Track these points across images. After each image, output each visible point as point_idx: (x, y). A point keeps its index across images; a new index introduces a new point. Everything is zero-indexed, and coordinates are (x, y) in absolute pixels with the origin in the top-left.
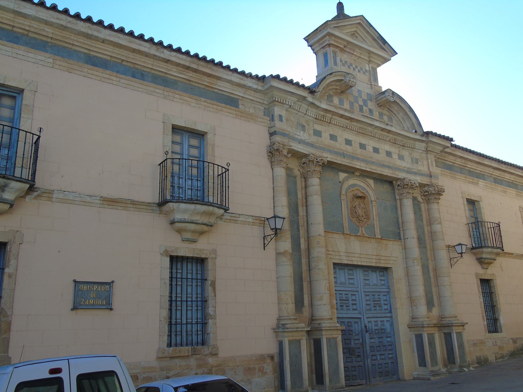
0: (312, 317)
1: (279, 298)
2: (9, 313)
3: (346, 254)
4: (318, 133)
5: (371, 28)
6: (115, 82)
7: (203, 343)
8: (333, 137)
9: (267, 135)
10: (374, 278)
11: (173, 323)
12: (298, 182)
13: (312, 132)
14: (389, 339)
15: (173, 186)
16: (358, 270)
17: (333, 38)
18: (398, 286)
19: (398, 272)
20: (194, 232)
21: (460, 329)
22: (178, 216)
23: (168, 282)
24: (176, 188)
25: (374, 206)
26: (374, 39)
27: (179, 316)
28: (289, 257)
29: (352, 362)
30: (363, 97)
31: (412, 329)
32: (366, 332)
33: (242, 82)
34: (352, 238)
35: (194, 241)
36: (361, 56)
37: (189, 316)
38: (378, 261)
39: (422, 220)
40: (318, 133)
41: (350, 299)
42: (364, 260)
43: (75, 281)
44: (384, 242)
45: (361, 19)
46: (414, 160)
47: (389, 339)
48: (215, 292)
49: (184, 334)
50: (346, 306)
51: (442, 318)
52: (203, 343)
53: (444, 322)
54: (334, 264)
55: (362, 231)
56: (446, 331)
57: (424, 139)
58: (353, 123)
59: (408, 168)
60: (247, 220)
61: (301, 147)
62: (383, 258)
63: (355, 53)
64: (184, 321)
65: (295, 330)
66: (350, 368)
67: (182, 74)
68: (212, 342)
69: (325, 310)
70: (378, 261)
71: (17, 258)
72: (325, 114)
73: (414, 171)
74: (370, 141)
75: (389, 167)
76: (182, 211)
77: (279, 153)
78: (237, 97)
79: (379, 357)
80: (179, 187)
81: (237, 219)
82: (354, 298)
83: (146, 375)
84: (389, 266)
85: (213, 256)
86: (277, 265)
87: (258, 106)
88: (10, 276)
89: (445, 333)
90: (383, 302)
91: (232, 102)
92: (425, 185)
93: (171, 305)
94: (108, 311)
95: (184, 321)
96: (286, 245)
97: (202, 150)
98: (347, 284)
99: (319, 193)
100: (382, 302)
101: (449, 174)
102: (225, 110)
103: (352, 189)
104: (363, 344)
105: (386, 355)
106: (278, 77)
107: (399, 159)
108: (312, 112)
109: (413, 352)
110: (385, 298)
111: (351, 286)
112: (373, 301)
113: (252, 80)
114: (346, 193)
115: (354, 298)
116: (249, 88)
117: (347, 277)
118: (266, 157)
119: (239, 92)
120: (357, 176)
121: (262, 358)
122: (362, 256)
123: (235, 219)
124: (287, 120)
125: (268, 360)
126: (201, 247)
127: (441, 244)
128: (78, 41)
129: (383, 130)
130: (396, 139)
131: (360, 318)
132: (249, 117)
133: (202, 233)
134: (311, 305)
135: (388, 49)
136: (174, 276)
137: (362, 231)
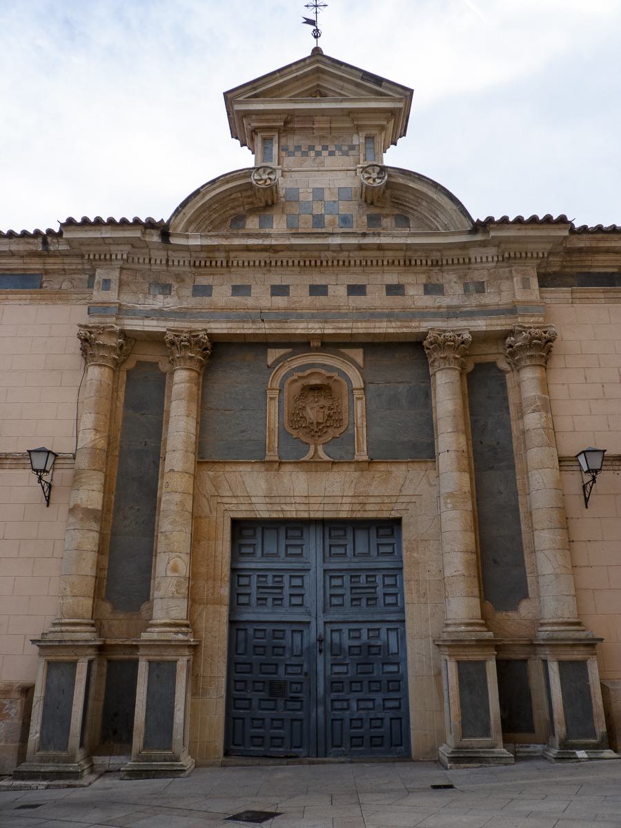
3: (268, 500)
8: (238, 290)
26: (358, 85)
42: (316, 507)
44: (382, 467)
57: (479, 237)
59: (448, 307)
61: (154, 323)
62: (372, 500)
70: (358, 507)
72: (210, 255)
75: (390, 316)
79: (354, 705)
82: (297, 582)
101: (602, 295)
102: (11, 296)
106: (70, 222)
110: (388, 581)
111: (294, 559)
114: (282, 385)
115: (297, 582)
119: (35, 265)
122: (312, 500)
135: (391, 90)
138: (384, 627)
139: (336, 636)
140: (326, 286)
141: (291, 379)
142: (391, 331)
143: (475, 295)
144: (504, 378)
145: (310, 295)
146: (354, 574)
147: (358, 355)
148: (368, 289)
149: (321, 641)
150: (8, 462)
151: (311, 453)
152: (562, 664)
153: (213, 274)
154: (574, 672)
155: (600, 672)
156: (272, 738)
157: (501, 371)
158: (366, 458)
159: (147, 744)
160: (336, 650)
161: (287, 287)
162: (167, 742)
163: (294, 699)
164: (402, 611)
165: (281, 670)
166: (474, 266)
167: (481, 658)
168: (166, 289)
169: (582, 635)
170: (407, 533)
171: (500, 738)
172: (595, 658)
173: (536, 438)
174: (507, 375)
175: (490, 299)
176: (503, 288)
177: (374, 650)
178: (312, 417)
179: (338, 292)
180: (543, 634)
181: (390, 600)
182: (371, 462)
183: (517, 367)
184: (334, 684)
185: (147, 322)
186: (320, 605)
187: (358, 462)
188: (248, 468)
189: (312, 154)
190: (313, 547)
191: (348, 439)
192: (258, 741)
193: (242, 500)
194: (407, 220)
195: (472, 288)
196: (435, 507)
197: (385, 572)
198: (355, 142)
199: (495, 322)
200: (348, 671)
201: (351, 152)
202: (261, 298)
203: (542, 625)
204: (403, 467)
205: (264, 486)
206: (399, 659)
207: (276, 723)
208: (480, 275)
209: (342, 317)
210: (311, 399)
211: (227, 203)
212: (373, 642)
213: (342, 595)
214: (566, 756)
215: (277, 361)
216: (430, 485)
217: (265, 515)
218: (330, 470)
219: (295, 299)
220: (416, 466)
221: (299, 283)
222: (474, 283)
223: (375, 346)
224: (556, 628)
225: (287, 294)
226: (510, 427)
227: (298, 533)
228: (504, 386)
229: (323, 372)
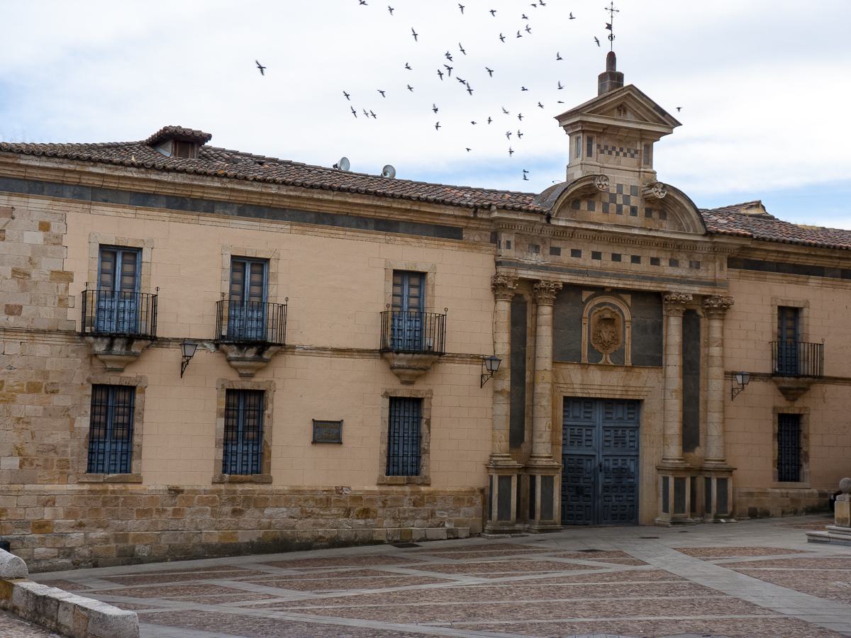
0: (532, 453)
1: (493, 436)
2: (270, 444)
3: (582, 387)
6: (341, 236)
7: (417, 474)
9: (493, 265)
10: (619, 412)
11: (391, 455)
12: (528, 308)
13: (548, 251)
14: (632, 480)
15: (393, 329)
20: (411, 376)
22: (396, 363)
23: (387, 420)
24: (396, 330)
25: (628, 327)
27: (396, 449)
28: (506, 396)
30: (615, 205)
31: (660, 471)
32: (601, 471)
35: (411, 383)
37: (406, 449)
38: (624, 393)
40: (555, 251)
41: (584, 435)
42: (605, 392)
43: (313, 420)
44: (637, 370)
45: (630, 89)
47: (632, 480)
48: (429, 430)
49: (401, 465)
50: (579, 442)
52: (417, 474)
53: (707, 466)
55: (606, 358)
56: (707, 476)
61: (532, 273)
62: (631, 389)
64: (401, 454)
67: (403, 215)
68: (424, 471)
69: (545, 447)
70: (624, 393)
71: (272, 403)
72: (565, 230)
75: (652, 279)
76: (401, 360)
79: (614, 499)
80: (398, 330)
82: (589, 433)
83: (369, 497)
84: (641, 398)
85: (429, 396)
86: (494, 403)
88: (269, 417)
89: (706, 478)
92: (705, 297)
93: (389, 440)
94: (337, 445)
95: (401, 454)
96: (505, 384)
97: (421, 300)
99: (550, 323)
101: (753, 276)
103: (599, 309)
105: (625, 497)
107: (671, 265)
109: (658, 495)
110: (632, 434)
111: (587, 420)
112: (615, 437)
114: (589, 315)
115: (589, 433)
118: (490, 291)
119: (462, 224)
121: (472, 492)
122: (603, 388)
124: (516, 244)
126: (419, 389)
128: (309, 205)
132: (475, 246)
133: (418, 377)
134: (531, 442)
136: (393, 414)
137: (606, 358)
138: (629, 458)
139: (607, 463)
140: (620, 255)
141: (594, 312)
142: (652, 288)
143: (695, 270)
144: (699, 320)
145: (612, 260)
146: (616, 429)
147: (628, 298)
148: (642, 258)
149: (600, 465)
150: (457, 359)
151: (604, 360)
152: (718, 479)
153: (561, 240)
154: (722, 483)
155: (733, 484)
156: (577, 515)
157: (698, 316)
158: (630, 364)
159: (542, 518)
160: (606, 470)
161: (600, 253)
162: (551, 517)
163: (588, 496)
164: (638, 450)
165: (581, 480)
166: (696, 251)
167: (684, 476)
168: (536, 249)
169: (726, 466)
170: (646, 409)
171: (689, 513)
172: (731, 477)
173: (717, 362)
174: (701, 319)
175: (702, 274)
176: (710, 268)
177: (624, 471)
178: (605, 337)
179: (626, 259)
180: (710, 465)
181: (632, 444)
182: (632, 367)
183: (710, 317)
184: (606, 488)
185: (530, 272)
186: (601, 446)
187: (626, 366)
188: (572, 367)
189: (614, 153)
190: (598, 415)
191: (621, 352)
192: (571, 517)
193: (569, 386)
194: (665, 214)
195: (694, 265)
196: (661, 391)
197: (631, 429)
198: (638, 148)
199: (703, 289)
200: (612, 481)
201: (636, 156)
202: (586, 261)
203: (706, 460)
204: (647, 370)
205: (580, 378)
206: (634, 475)
207: (579, 508)
208: (698, 257)
209: (627, 277)
210: (603, 325)
211: (582, 193)
212: (624, 467)
213: (610, 441)
214: (717, 521)
215: (588, 300)
216: (659, 382)
217: (580, 395)
218: (612, 370)
219: (604, 262)
220: (653, 370)
221: (606, 252)
222: (695, 262)
223: (637, 294)
224: (717, 463)
225: (600, 258)
226: (699, 350)
227: (590, 405)
228: (698, 325)
229: (611, 308)
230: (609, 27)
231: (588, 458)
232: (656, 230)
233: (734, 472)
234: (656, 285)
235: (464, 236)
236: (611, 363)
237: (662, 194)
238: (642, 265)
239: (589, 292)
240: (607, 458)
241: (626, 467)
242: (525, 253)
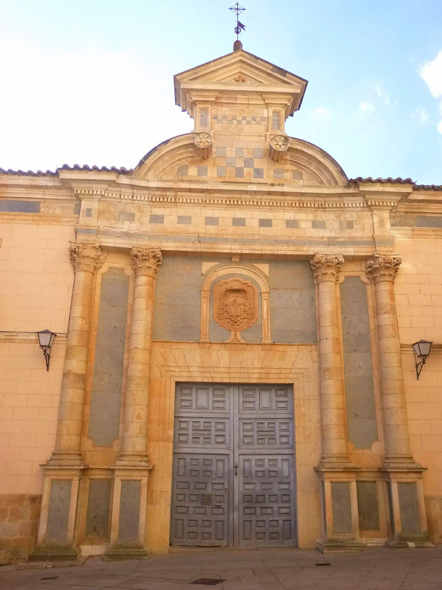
3: (201, 369)
4: (156, 219)
5: (259, 61)
10: (265, 399)
14: (286, 486)
16: (232, 390)
17: (194, 93)
18: (302, 409)
19: (305, 390)
21: (410, 478)
29: (205, 514)
33: (33, 183)
34: (216, 347)
36: (250, 102)
38: (263, 376)
39: (367, 309)
44: (280, 348)
46: (345, 225)
47: (286, 486)
51: (387, 458)
54: (177, 383)
57: (351, 191)
58: (213, 195)
60: (28, 338)
63: (238, 102)
65: (58, 468)
66: (200, 522)
70: (263, 376)
72: (164, 193)
73: (342, 240)
74: (254, 213)
75: (288, 243)
77: (78, 255)
78: (37, 200)
81: (15, 338)
82: (220, 427)
87: (67, 204)
90: (279, 433)
91: (29, 207)
98: (210, 408)
100: (278, 433)
101: (432, 233)
104: (230, 491)
108: (143, 196)
110: (284, 427)
113: (45, 178)
115: (220, 427)
116: (46, 187)
117: (274, 399)
119: (36, 195)
120: (236, 262)
123: (12, 338)
125: (26, 503)
127: (390, 344)
129: (270, 193)
130: (317, 202)
131: (228, 455)
132: (54, 219)
135: (292, 80)
139: (247, 464)
165: (209, 487)
181: (284, 440)
186: (236, 442)
189: (235, 122)
213: (252, 436)
227: (221, 393)
230: (240, 26)
231: (219, 457)
232: (279, 185)
233: (425, 473)
234: (294, 248)
235: (42, 210)
236: (243, 341)
237: (283, 147)
238: (274, 228)
239: (209, 263)
240: (246, 457)
241: (276, 469)
242: (113, 221)
